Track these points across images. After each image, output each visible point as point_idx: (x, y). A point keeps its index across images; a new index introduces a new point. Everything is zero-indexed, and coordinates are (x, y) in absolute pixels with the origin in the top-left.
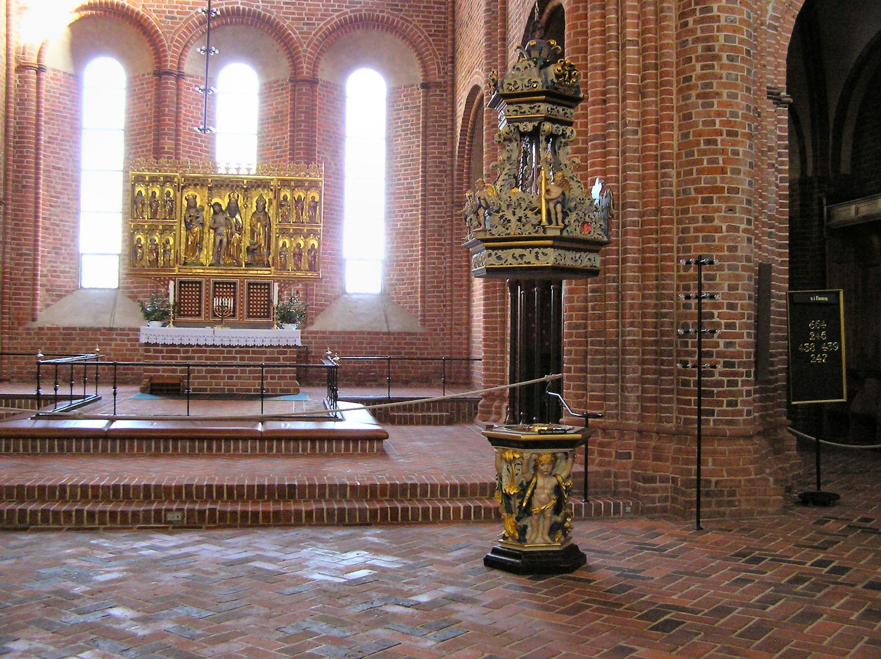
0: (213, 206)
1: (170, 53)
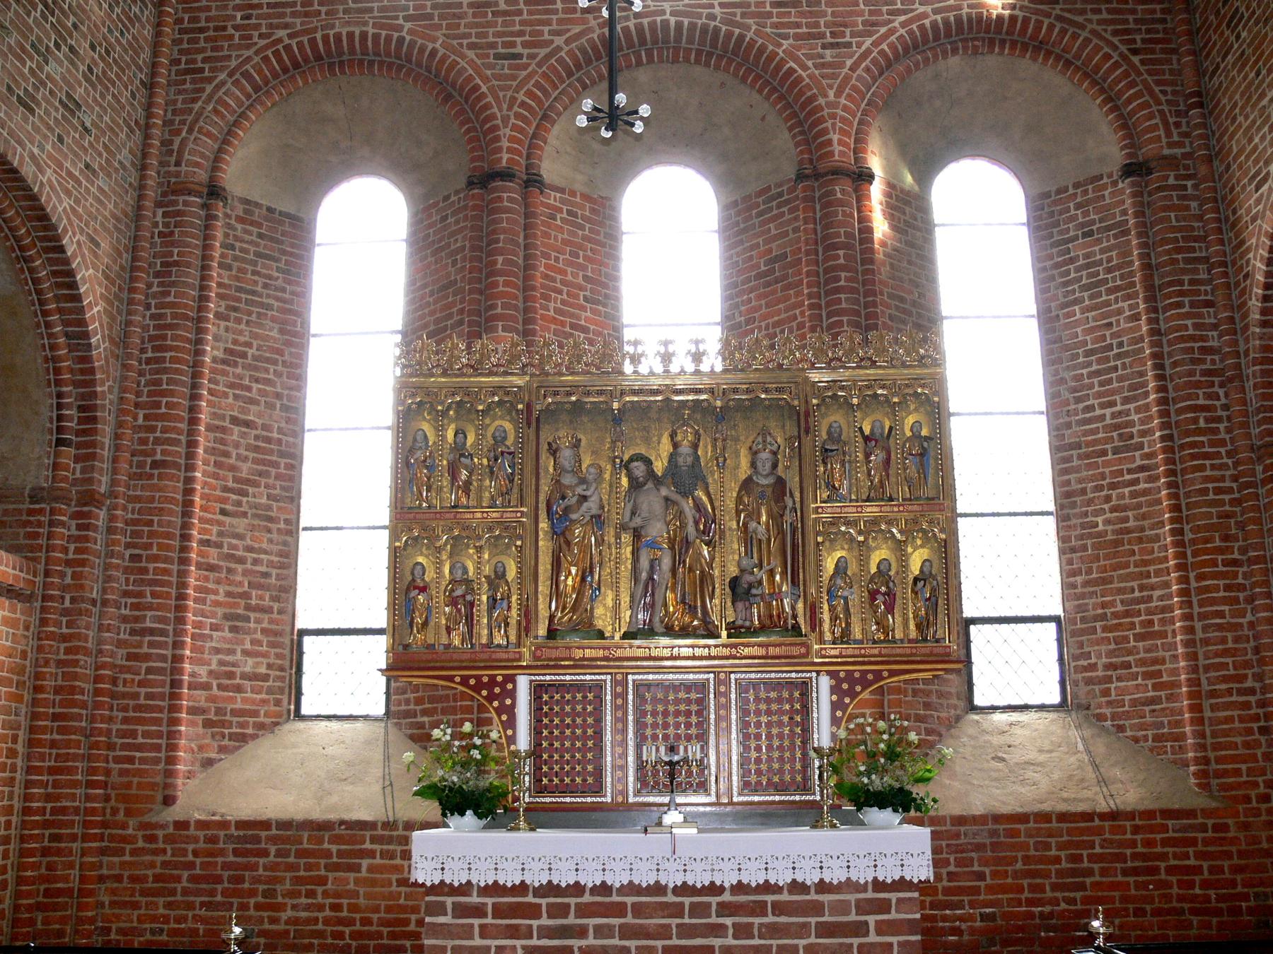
0: (626, 466)
1: (508, 131)
